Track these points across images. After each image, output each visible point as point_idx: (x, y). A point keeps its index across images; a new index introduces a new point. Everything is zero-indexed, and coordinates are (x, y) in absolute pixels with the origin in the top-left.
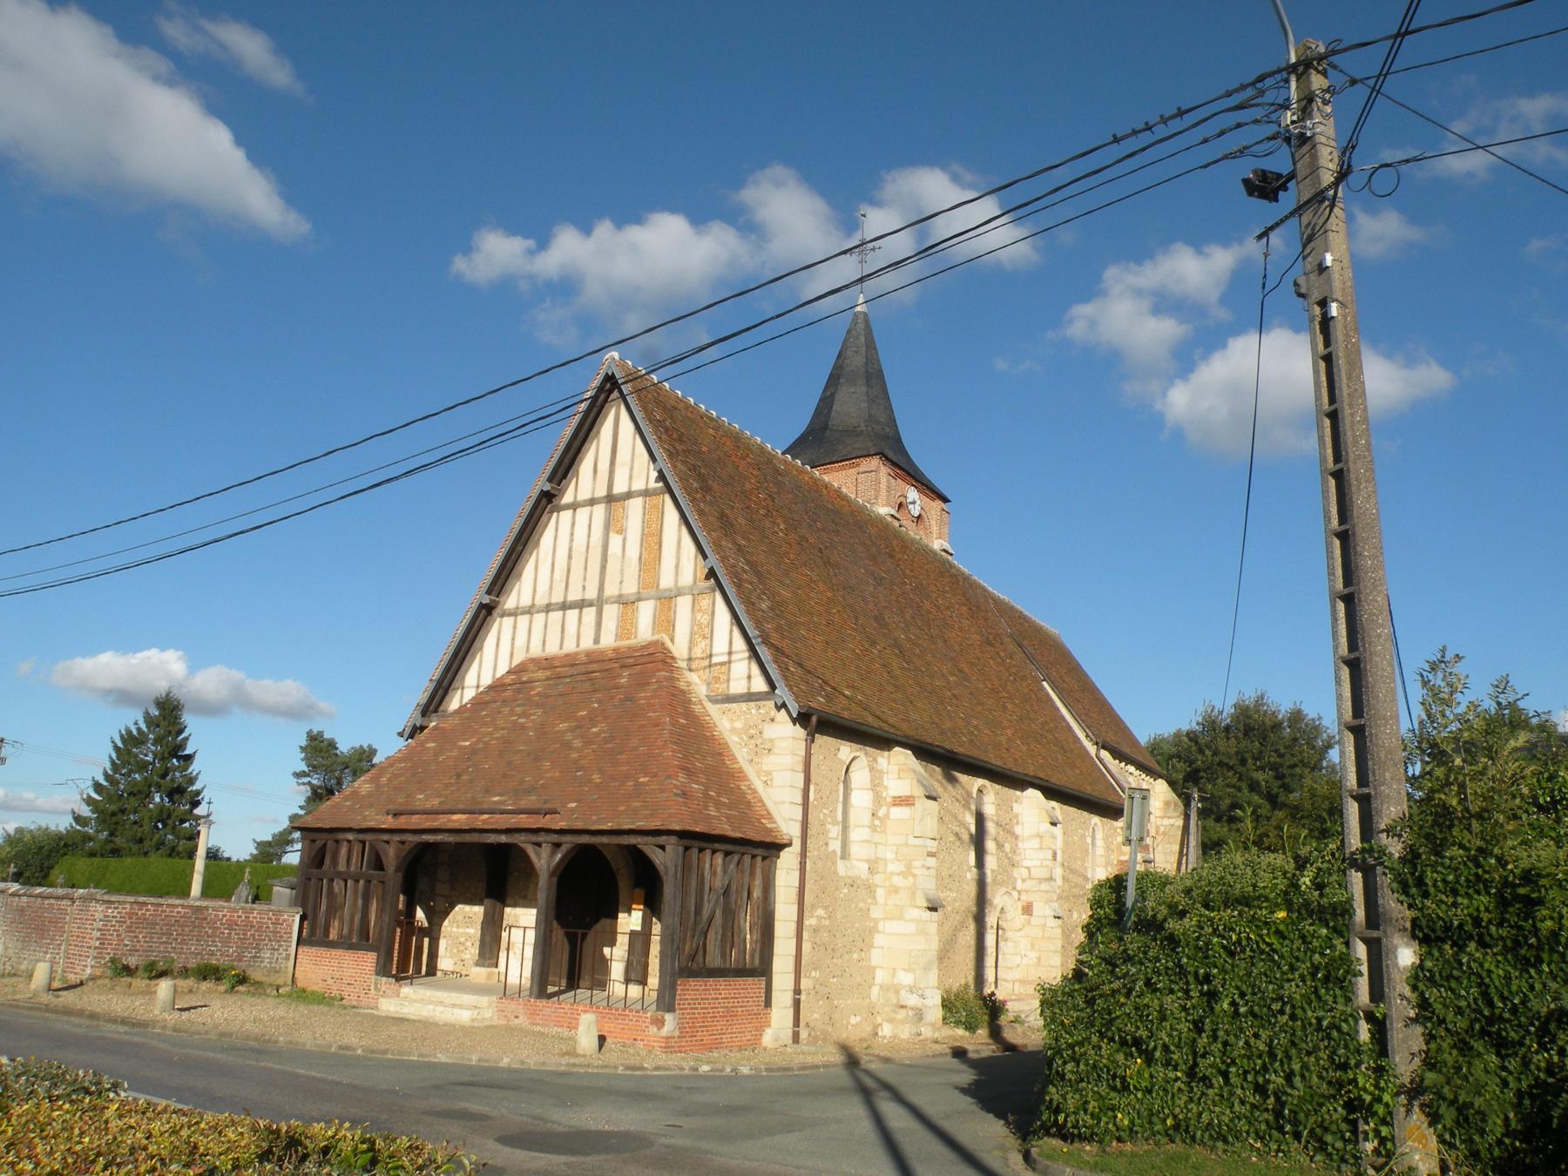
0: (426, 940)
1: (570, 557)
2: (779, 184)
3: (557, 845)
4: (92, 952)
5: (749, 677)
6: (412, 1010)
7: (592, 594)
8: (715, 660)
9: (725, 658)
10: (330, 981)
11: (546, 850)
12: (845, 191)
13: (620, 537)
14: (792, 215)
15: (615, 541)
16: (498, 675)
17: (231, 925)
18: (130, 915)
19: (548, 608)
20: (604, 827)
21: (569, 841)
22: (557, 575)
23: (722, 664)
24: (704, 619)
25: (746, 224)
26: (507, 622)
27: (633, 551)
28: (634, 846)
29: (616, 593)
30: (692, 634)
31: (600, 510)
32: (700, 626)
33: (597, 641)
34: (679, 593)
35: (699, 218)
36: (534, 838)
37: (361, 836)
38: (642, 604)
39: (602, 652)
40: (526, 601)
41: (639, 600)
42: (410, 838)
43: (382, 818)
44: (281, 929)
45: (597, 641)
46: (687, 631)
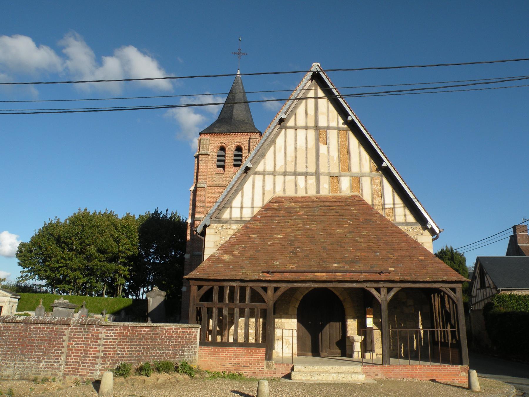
0: (443, 341)
1: (296, 151)
2: (76, 39)
3: (389, 290)
4: (100, 361)
5: (405, 215)
6: (320, 378)
7: (312, 169)
8: (386, 206)
9: (392, 206)
10: (228, 365)
11: (384, 291)
12: (102, 50)
13: (326, 146)
14: (79, 53)
15: (323, 149)
16: (265, 203)
17: (170, 337)
18: (120, 334)
19: (285, 174)
20: (425, 280)
21: (397, 287)
22: (289, 159)
23: (390, 208)
24: (378, 188)
25: (60, 52)
26: (259, 179)
27: (334, 153)
28: (363, 289)
29: (327, 171)
30: (373, 195)
31: (312, 133)
32: (376, 191)
33: (318, 191)
34: (363, 175)
35: (39, 42)
36: (376, 285)
37: (243, 284)
38: (342, 178)
39: (309, 197)
40: (270, 168)
41: (341, 176)
42: (284, 285)
43: (261, 274)
44: (192, 337)
45: (318, 191)
46: (370, 193)
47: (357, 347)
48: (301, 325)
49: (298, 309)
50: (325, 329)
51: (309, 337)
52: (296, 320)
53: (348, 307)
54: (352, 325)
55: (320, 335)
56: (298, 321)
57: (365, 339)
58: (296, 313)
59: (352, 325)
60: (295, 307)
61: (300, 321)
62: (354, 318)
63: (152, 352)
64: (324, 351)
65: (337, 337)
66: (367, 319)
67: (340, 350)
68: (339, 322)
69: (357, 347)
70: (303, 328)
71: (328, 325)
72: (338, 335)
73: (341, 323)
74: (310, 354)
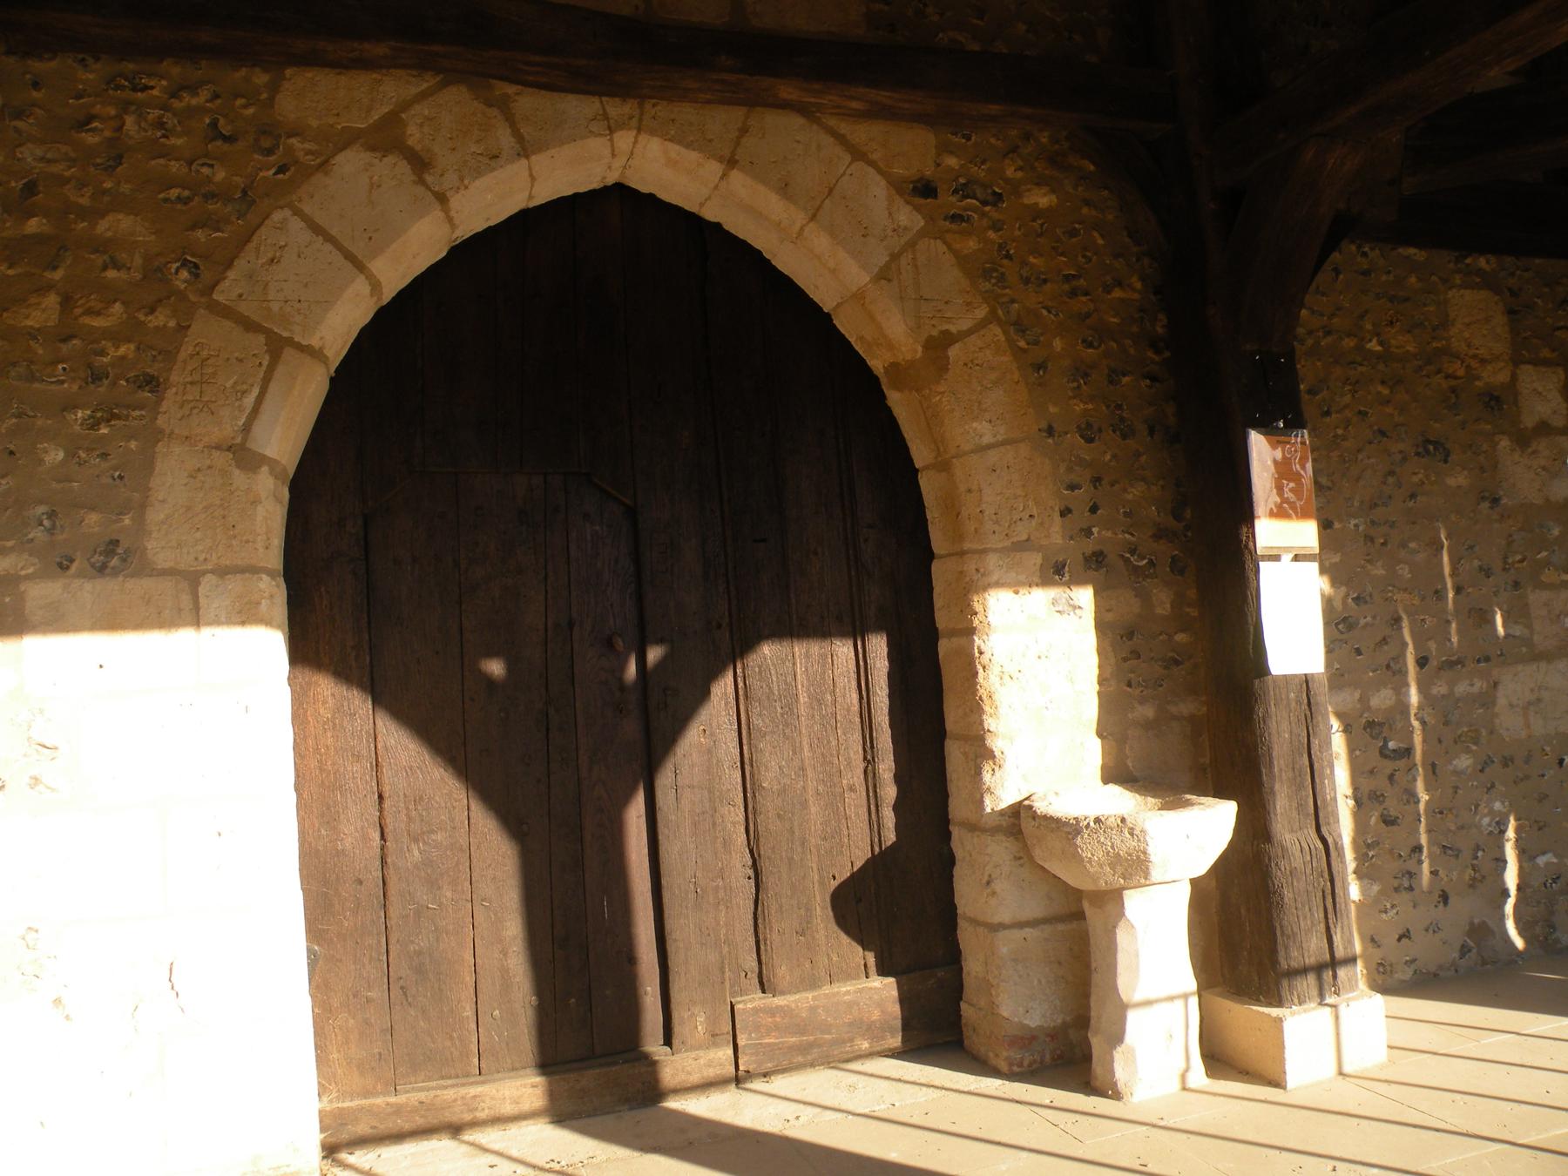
47: (1155, 950)
48: (359, 703)
49: (307, 487)
50: (694, 737)
51: (495, 858)
52: (263, 649)
53: (980, 441)
54: (1040, 669)
55: (635, 813)
56: (302, 653)
57: (1254, 832)
58: (272, 553)
59: (1040, 669)
60: (244, 456)
61: (318, 642)
62: (1055, 573)
63: (330, 741)
64: (694, 1020)
65: (841, 813)
66: (843, 650)
67: (885, 988)
68: (856, 631)
69: (1155, 950)
70: (402, 747)
71: (723, 688)
72: (856, 804)
73: (878, 646)
74: (528, 1089)
